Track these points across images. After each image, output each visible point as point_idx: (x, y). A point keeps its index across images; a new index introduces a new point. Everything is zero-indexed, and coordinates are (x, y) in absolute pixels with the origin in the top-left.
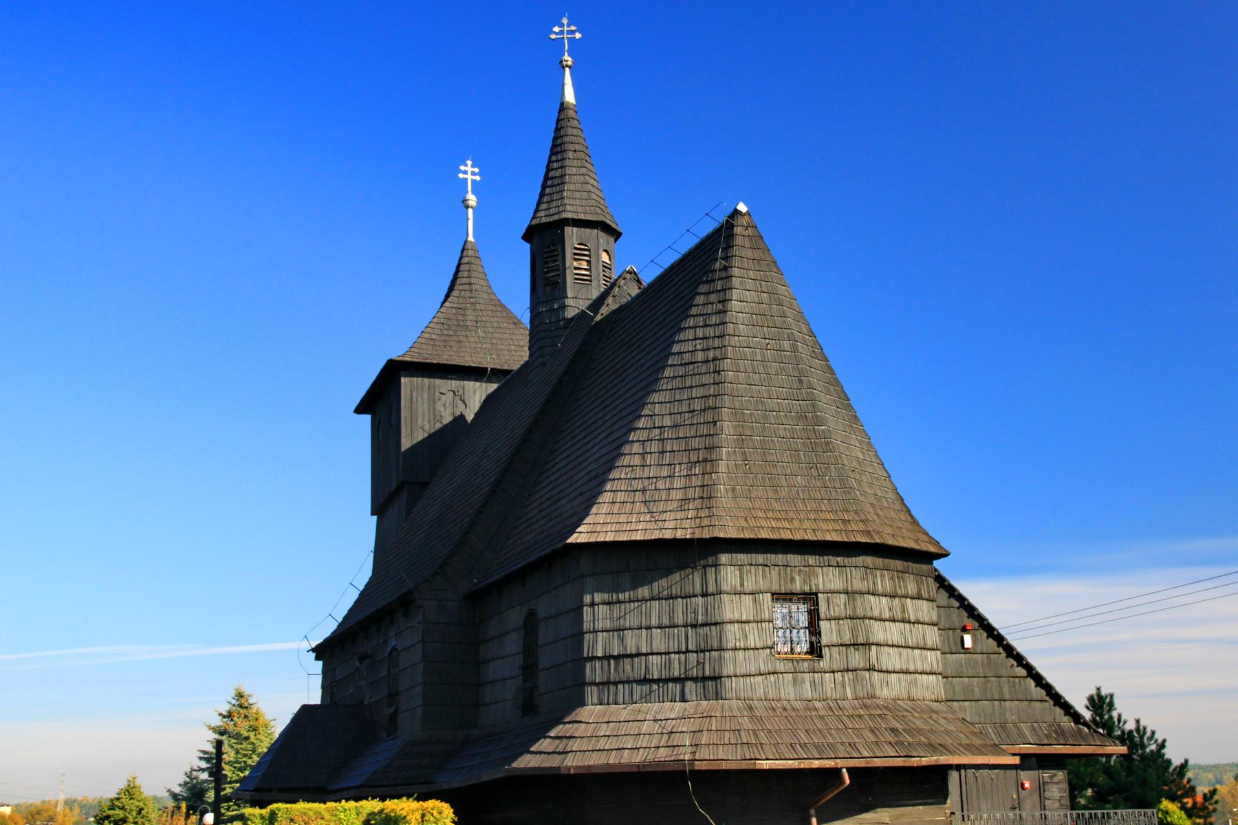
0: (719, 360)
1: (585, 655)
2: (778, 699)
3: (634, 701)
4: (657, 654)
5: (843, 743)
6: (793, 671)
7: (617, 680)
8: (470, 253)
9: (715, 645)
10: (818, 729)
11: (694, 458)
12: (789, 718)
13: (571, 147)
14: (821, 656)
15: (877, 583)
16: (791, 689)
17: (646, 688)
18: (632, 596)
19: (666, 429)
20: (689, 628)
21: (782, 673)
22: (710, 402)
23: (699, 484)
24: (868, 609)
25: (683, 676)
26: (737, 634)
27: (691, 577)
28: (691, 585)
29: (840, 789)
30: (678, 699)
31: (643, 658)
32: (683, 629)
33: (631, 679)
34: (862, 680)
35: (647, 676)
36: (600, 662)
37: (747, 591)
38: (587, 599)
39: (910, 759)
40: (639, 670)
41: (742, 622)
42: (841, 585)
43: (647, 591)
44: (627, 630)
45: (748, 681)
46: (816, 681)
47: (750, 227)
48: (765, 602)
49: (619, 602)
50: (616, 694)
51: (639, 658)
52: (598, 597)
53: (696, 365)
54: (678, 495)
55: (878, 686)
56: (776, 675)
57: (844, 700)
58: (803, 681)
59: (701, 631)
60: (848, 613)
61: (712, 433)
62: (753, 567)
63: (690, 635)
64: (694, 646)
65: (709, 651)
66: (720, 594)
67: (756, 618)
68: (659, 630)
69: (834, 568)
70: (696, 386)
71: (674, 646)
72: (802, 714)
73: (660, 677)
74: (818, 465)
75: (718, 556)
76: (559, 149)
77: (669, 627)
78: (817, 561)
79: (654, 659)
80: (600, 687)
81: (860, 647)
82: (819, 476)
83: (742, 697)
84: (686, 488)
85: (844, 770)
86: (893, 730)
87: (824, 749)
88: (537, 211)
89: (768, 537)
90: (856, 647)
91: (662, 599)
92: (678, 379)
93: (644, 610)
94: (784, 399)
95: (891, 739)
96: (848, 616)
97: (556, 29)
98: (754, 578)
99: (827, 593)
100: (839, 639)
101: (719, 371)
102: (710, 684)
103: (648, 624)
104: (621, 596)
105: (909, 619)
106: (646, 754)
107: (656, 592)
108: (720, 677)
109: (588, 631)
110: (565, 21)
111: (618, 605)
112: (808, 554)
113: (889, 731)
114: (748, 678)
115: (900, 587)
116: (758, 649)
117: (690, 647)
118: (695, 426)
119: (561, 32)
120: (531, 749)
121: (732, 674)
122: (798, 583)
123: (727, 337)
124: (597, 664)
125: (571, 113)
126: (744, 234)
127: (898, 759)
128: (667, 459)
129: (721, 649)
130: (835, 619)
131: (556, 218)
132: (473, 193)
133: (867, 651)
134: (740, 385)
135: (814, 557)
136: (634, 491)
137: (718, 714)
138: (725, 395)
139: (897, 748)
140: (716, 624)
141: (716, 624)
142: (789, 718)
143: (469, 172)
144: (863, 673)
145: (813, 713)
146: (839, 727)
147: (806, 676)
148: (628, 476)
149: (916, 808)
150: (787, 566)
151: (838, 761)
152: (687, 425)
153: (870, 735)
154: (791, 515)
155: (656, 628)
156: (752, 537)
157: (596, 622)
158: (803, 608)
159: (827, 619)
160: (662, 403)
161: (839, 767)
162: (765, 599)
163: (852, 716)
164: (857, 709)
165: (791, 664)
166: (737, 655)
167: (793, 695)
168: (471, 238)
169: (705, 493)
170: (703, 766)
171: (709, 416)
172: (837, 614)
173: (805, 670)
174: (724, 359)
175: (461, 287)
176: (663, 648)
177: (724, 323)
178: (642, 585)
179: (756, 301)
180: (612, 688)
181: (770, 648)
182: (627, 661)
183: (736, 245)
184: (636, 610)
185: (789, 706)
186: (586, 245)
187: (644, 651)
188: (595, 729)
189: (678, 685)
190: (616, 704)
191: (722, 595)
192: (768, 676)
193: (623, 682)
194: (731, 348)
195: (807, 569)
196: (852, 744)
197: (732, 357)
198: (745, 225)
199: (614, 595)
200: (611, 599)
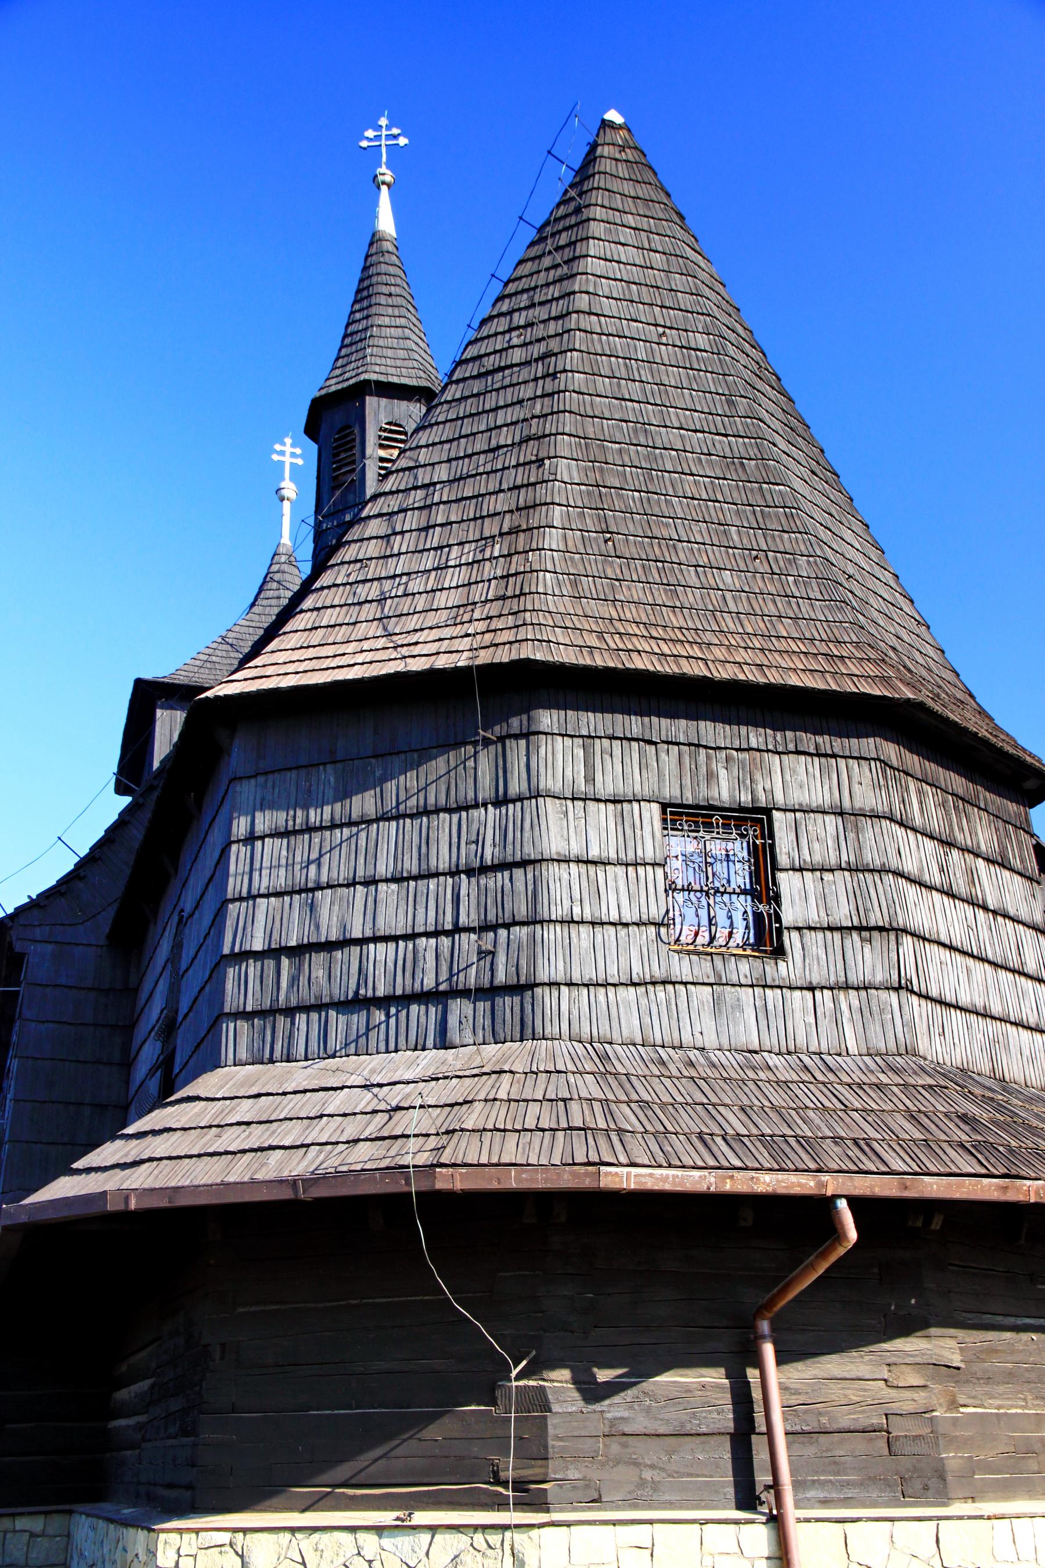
0: (556, 355)
1: (226, 950)
2: (677, 1043)
3: (330, 1052)
4: (386, 939)
5: (837, 1139)
6: (712, 980)
7: (294, 1003)
9: (522, 911)
10: (773, 1107)
11: (491, 528)
12: (701, 1083)
13: (385, 290)
14: (779, 952)
15: (911, 804)
16: (708, 1023)
17: (358, 1020)
18: (337, 817)
19: (438, 487)
20: (463, 876)
21: (685, 984)
22: (535, 427)
23: (499, 573)
24: (892, 852)
25: (442, 988)
26: (576, 888)
27: (470, 763)
28: (471, 781)
29: (833, 1258)
30: (430, 1043)
31: (355, 950)
32: (450, 880)
33: (326, 1000)
34: (882, 1011)
35: (362, 992)
36: (259, 964)
37: (601, 794)
38: (240, 827)
39: (1019, 1182)
40: (345, 977)
41: (587, 862)
42: (827, 796)
43: (373, 800)
44: (322, 888)
45: (601, 998)
46: (770, 1007)
47: (630, 148)
48: (646, 822)
49: (310, 829)
50: (291, 1036)
51: (346, 950)
52: (264, 821)
53: (507, 372)
54: (455, 598)
55: (921, 1028)
56: (670, 987)
57: (840, 1055)
58: (739, 1006)
59: (490, 881)
60: (844, 858)
61: (532, 480)
62: (616, 744)
63: (463, 892)
64: (473, 916)
65: (507, 926)
66: (536, 797)
67: (622, 856)
68: (394, 887)
69: (809, 759)
70: (506, 406)
71: (424, 919)
72: (734, 1075)
73: (392, 993)
74: (770, 554)
75: (533, 713)
76: (365, 293)
77: (415, 878)
78: (770, 740)
79: (380, 951)
80: (256, 1020)
81: (876, 934)
82: (773, 573)
83: (586, 1036)
84: (470, 584)
85: (842, 1204)
86: (964, 1118)
87: (788, 1150)
89: (651, 668)
90: (865, 934)
91: (405, 816)
92: (469, 401)
93: (362, 843)
94: (696, 431)
95: (965, 1137)
96: (844, 865)
97: (370, 133)
98: (618, 767)
99: (794, 811)
100: (823, 914)
101: (555, 373)
102: (508, 1004)
103: (370, 872)
104: (314, 816)
105: (469, 877)
106: (322, 1157)
107: (390, 803)
108: (532, 986)
109: (237, 896)
110: (383, 122)
111: (307, 836)
112: (747, 724)
113: (957, 1120)
114: (602, 990)
115: (961, 829)
116: (626, 925)
117: (463, 920)
118: (499, 474)
119: (378, 138)
120: (75, 1166)
121: (560, 978)
122: (724, 784)
123: (574, 316)
124: (251, 970)
125: (388, 246)
126: (618, 156)
127: (986, 1181)
128: (436, 537)
129: (534, 921)
130: (813, 870)
131: (351, 382)
132: (291, 480)
133: (893, 945)
134: (598, 399)
135: (761, 730)
136: (360, 604)
137: (518, 1067)
138: (564, 411)
139: (979, 1156)
140: (524, 863)
141: (524, 863)
142: (701, 1083)
144: (883, 995)
145: (762, 1075)
146: (827, 1104)
147: (746, 995)
148: (351, 579)
149: (1025, 1336)
150: (698, 746)
151: (825, 1177)
152: (481, 474)
153: (907, 1126)
154: (709, 637)
155: (387, 881)
156: (611, 664)
157: (256, 875)
158: (739, 849)
159: (794, 869)
160: (434, 444)
161: (829, 1193)
162: (646, 816)
163: (859, 1086)
164: (872, 1072)
165: (709, 964)
166: (574, 935)
167: (714, 1036)
168: (286, 540)
169: (510, 588)
170: (458, 1177)
171: (529, 453)
172: (817, 858)
173: (743, 981)
174: (565, 352)
175: (265, 602)
176: (401, 923)
177: (569, 294)
178: (362, 789)
179: (637, 263)
180: (281, 1021)
181: (658, 925)
182: (319, 959)
183: (599, 173)
184: (344, 845)
185: (702, 1060)
186: (400, 426)
187: (357, 934)
188: (222, 1111)
189: (432, 1010)
190: (288, 1061)
191: (541, 800)
192: (650, 988)
193: (307, 1009)
194: (583, 334)
195: (745, 755)
196: (862, 1143)
197: (584, 348)
198: (621, 143)
199: (299, 813)
200: (291, 823)
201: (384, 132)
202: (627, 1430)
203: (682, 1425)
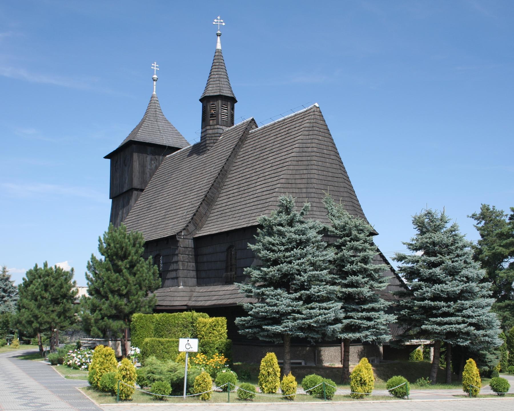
8: (155, 99)
88: (206, 88)
97: (216, 20)
110: (219, 18)
119: (217, 22)
120: (170, 269)
143: (155, 66)
201: (219, 21)
202: (149, 397)
203: (113, 380)
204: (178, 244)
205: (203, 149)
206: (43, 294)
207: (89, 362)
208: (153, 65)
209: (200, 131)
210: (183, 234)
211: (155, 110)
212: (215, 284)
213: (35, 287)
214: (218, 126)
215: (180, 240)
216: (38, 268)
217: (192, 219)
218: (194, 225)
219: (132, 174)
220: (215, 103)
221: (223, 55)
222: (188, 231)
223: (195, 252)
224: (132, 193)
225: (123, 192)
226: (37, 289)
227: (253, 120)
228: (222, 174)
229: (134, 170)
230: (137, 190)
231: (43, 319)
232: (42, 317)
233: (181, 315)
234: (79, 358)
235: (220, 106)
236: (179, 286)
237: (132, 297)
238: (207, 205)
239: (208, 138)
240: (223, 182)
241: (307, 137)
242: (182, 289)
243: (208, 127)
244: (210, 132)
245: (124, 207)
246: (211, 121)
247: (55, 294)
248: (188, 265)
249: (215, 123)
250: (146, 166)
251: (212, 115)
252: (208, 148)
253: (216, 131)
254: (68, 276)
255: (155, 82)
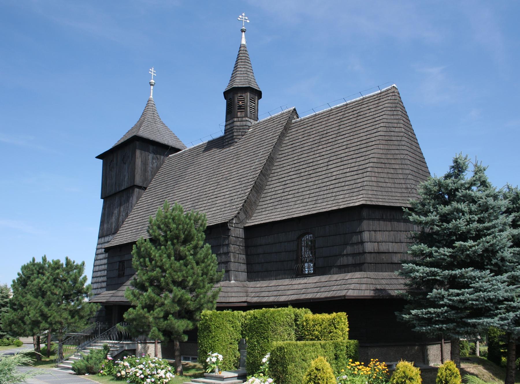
97: (240, 17)
119: (242, 18)
204: (228, 233)
205: (228, 141)
206: (53, 290)
207: (156, 373)
208: (150, 70)
209: (224, 124)
210: (234, 222)
211: (152, 112)
212: (278, 277)
213: (42, 282)
214: (247, 118)
215: (232, 228)
216: (36, 262)
217: (243, 206)
218: (245, 213)
219: (134, 171)
220: (244, 95)
221: (247, 50)
222: (239, 219)
223: (245, 242)
224: (134, 190)
225: (121, 190)
226: (45, 283)
227: (295, 110)
228: (269, 161)
229: (136, 167)
230: (140, 187)
231: (54, 318)
232: (52, 316)
233: (284, 311)
234: (141, 369)
235: (248, 99)
236: (230, 281)
237: (199, 290)
238: (256, 192)
239: (236, 130)
240: (271, 170)
241: (392, 117)
242: (234, 284)
243: (235, 119)
244: (238, 124)
245: (120, 205)
246: (239, 113)
247: (67, 290)
248: (239, 257)
249: (243, 115)
250: (148, 165)
251: (240, 107)
252: (236, 140)
253: (244, 123)
254: (80, 268)
255: (152, 87)
